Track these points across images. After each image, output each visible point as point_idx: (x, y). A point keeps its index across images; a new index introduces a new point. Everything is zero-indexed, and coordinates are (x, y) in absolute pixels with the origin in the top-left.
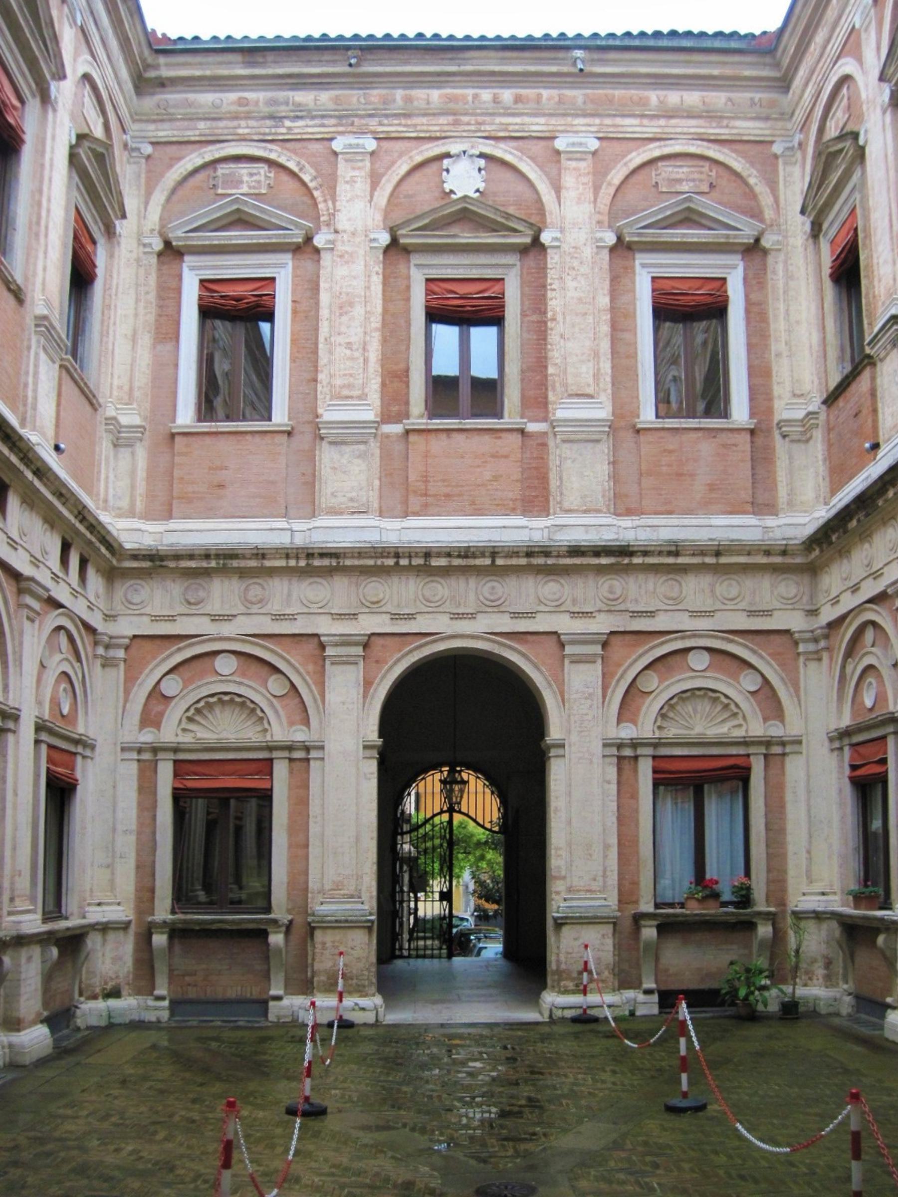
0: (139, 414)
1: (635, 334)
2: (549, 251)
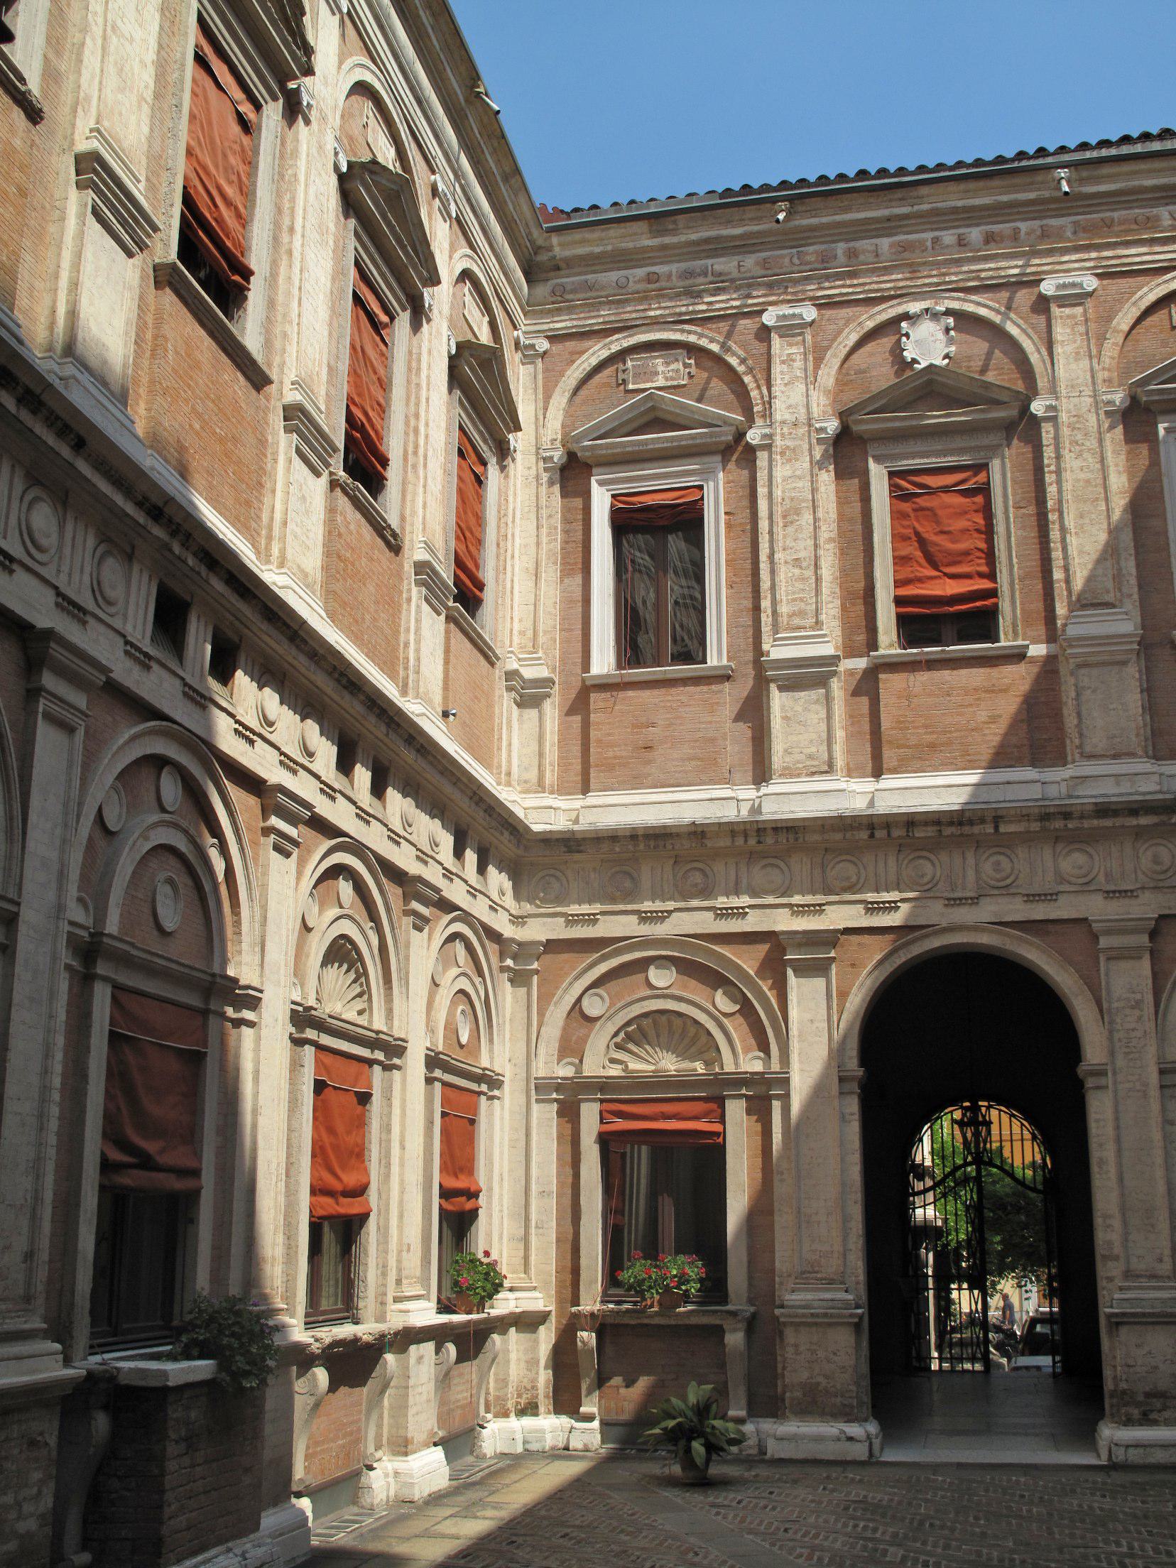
0: (547, 665)
1: (1165, 520)
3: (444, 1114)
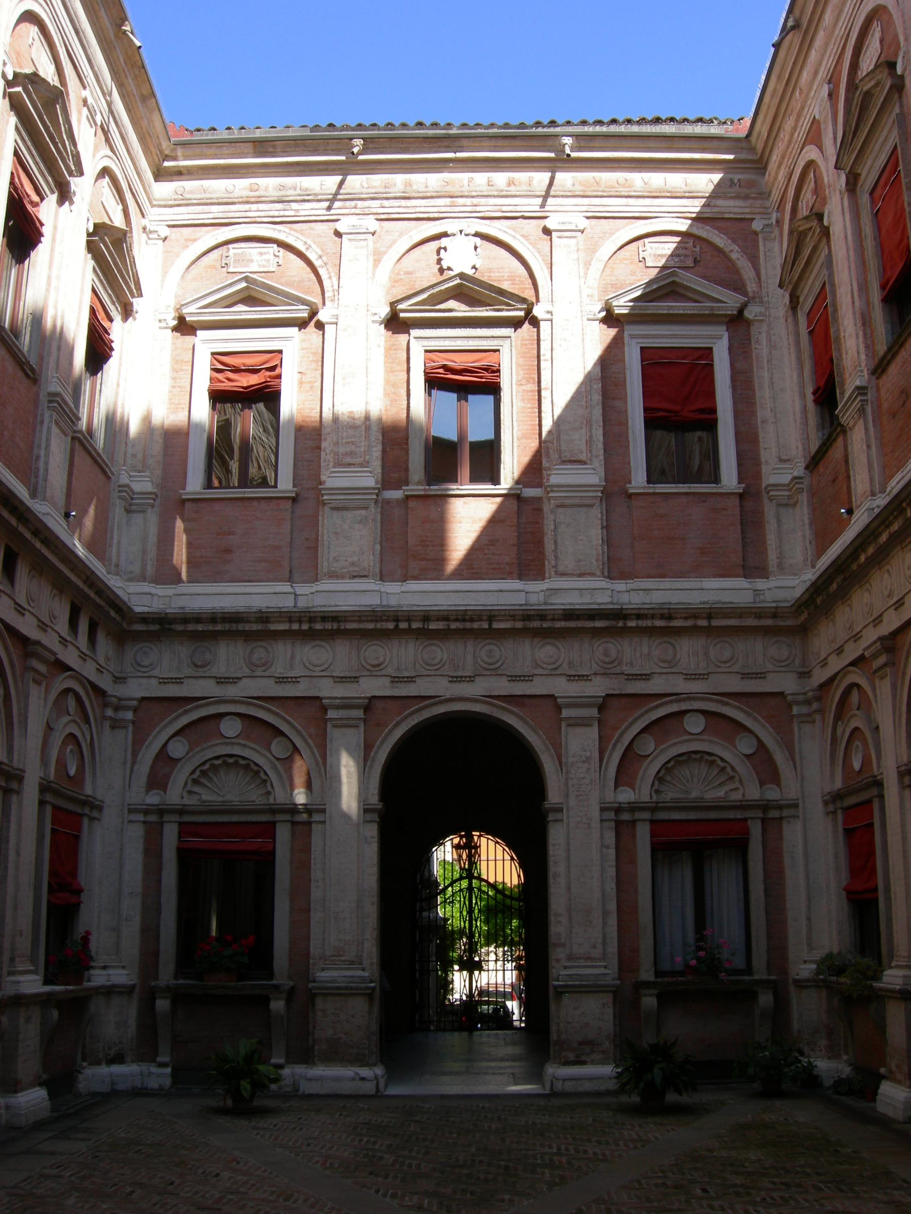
0: (152, 482)
1: (626, 402)
2: (541, 323)
3: (53, 830)
